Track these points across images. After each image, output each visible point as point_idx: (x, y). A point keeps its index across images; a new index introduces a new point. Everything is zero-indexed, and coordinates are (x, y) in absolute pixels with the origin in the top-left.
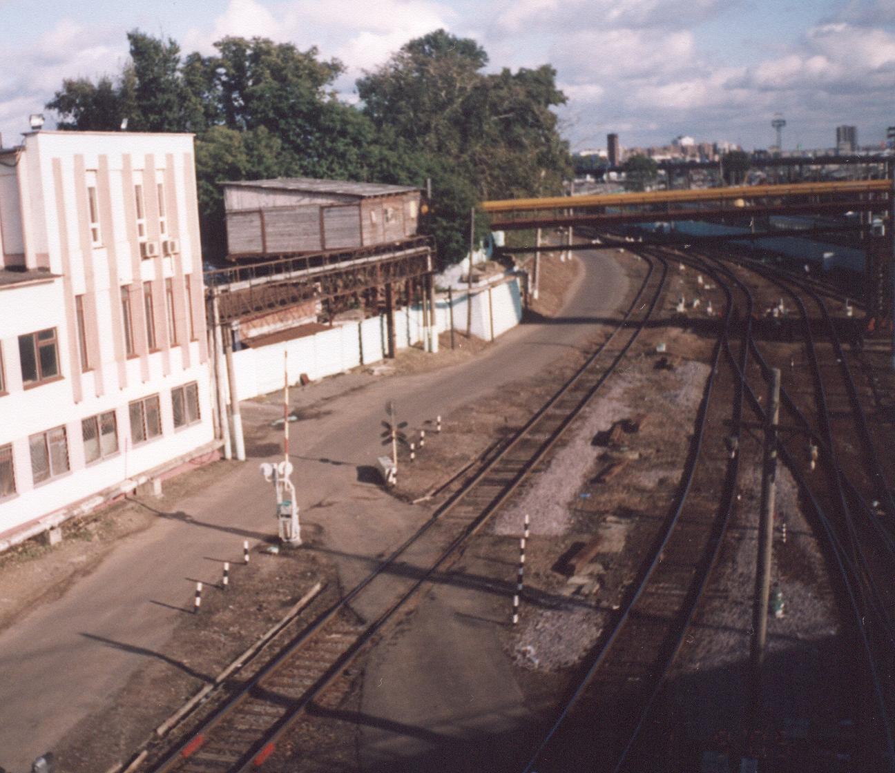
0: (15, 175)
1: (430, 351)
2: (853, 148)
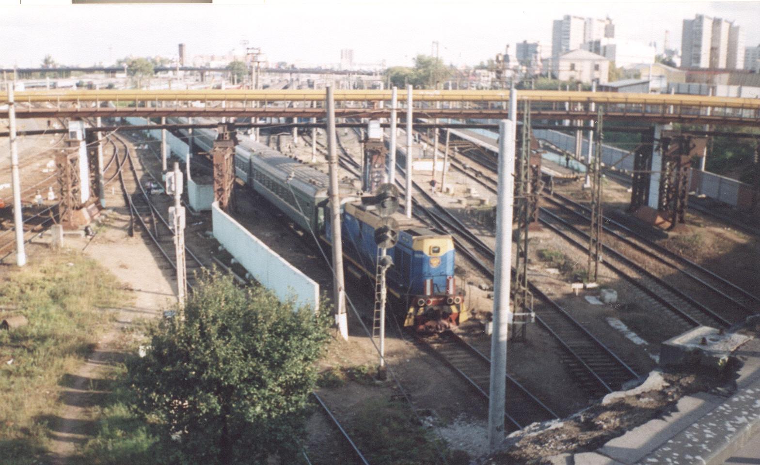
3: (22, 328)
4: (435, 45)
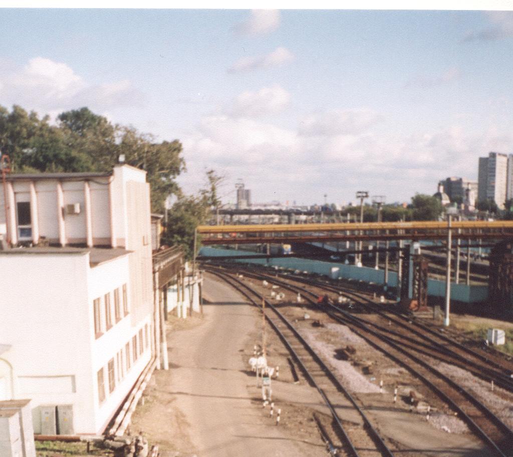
0: (108, 190)
1: (182, 317)
2: (249, 205)
3: (136, 132)
4: (146, 243)
